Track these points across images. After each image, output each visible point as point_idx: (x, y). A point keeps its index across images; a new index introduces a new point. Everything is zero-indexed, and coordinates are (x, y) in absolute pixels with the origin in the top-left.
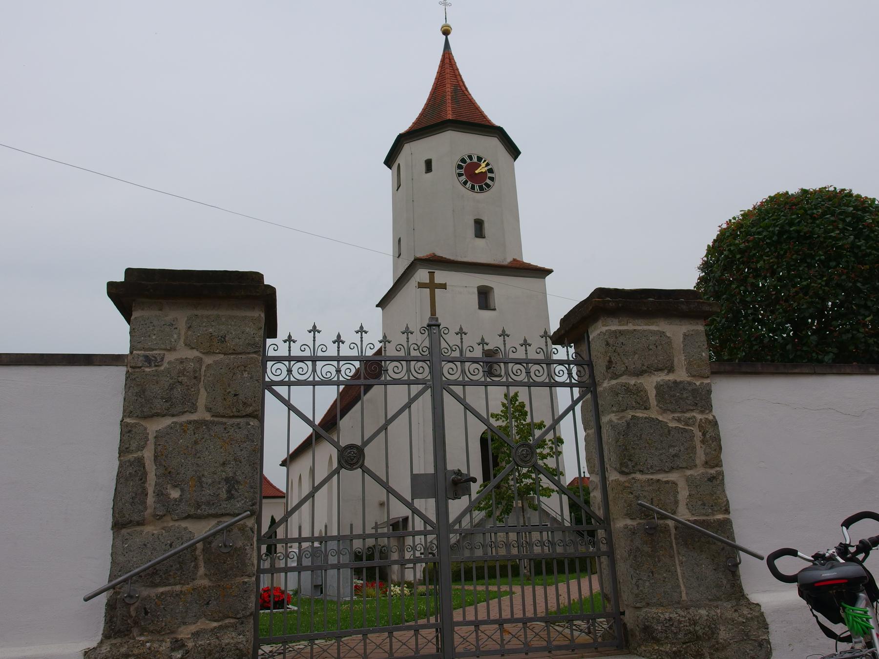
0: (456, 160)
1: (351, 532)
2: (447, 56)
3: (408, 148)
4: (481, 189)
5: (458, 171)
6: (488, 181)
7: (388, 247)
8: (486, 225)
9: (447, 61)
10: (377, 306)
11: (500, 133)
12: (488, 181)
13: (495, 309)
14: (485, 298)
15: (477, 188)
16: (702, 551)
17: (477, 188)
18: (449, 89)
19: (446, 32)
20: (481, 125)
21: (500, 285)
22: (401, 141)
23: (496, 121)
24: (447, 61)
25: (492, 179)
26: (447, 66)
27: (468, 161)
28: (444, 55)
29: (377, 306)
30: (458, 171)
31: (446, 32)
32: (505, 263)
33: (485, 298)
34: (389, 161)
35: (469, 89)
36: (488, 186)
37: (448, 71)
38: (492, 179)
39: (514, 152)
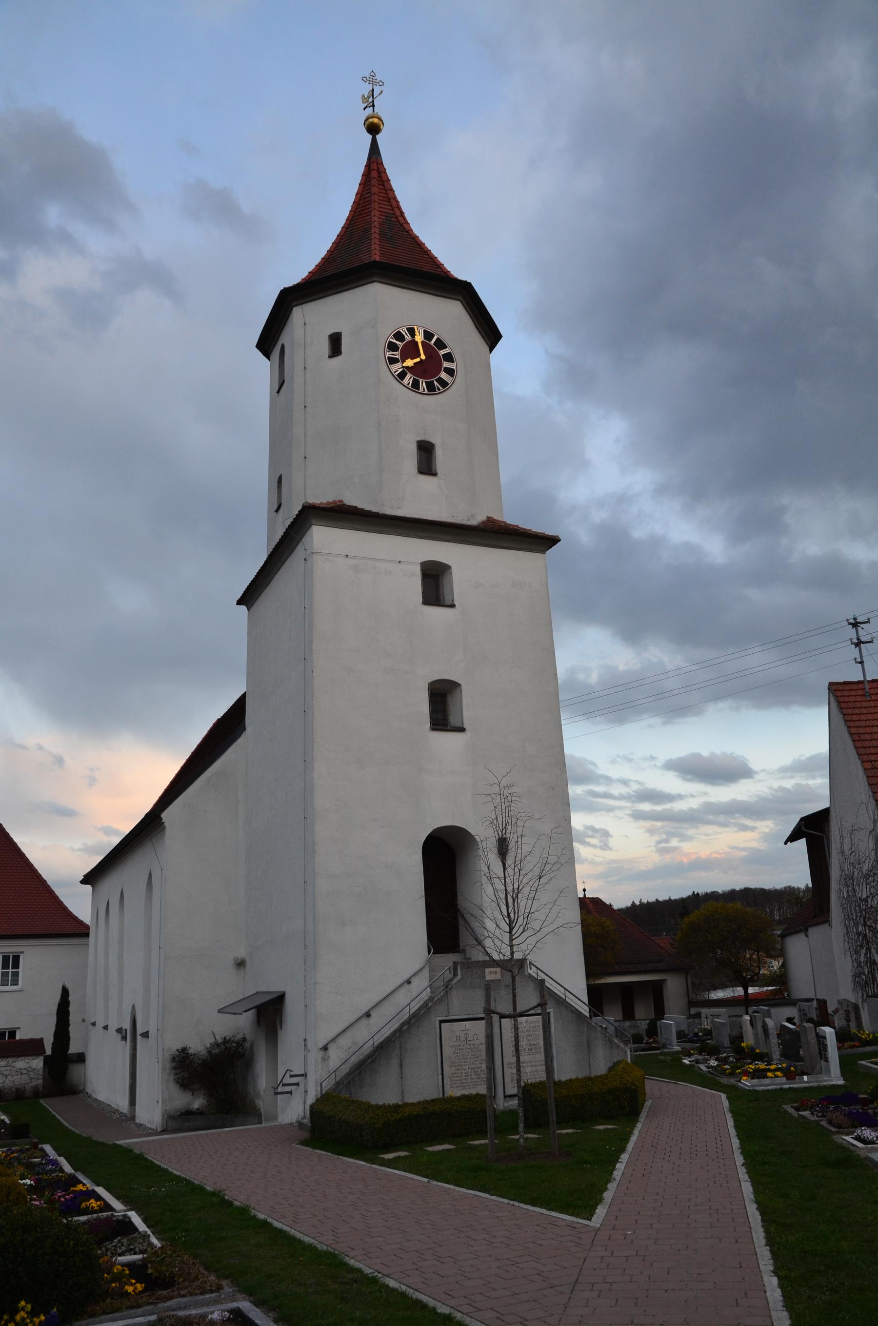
0: (386, 335)
1: (549, 1070)
2: (374, 166)
3: (299, 314)
4: (431, 388)
5: (389, 354)
6: (443, 375)
7: (463, 692)
8: (439, 454)
9: (374, 174)
10: (239, 602)
11: (465, 293)
12: (443, 375)
13: (453, 606)
14: (435, 583)
15: (423, 385)
16: (9, 1188)
17: (423, 385)
18: (376, 219)
19: (373, 129)
20: (424, 274)
21: (465, 562)
22: (288, 300)
23: (458, 272)
24: (374, 174)
25: (451, 372)
26: (374, 182)
27: (408, 338)
28: (368, 166)
29: (239, 602)
30: (389, 354)
31: (373, 129)
32: (474, 522)
33: (435, 583)
34: (269, 341)
35: (406, 215)
36: (444, 384)
37: (375, 190)
38: (451, 372)
39: (491, 335)
